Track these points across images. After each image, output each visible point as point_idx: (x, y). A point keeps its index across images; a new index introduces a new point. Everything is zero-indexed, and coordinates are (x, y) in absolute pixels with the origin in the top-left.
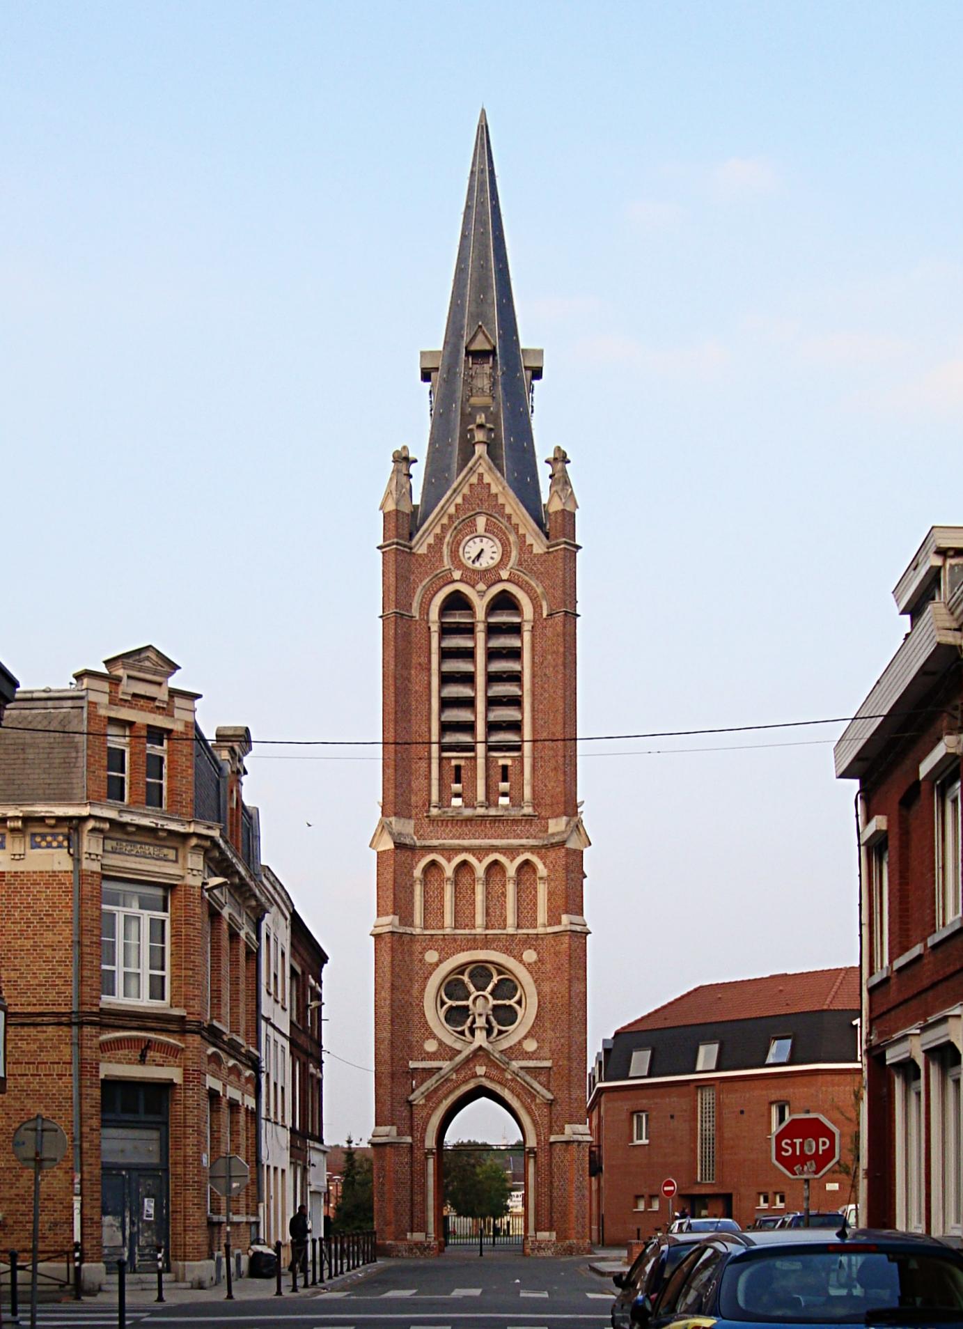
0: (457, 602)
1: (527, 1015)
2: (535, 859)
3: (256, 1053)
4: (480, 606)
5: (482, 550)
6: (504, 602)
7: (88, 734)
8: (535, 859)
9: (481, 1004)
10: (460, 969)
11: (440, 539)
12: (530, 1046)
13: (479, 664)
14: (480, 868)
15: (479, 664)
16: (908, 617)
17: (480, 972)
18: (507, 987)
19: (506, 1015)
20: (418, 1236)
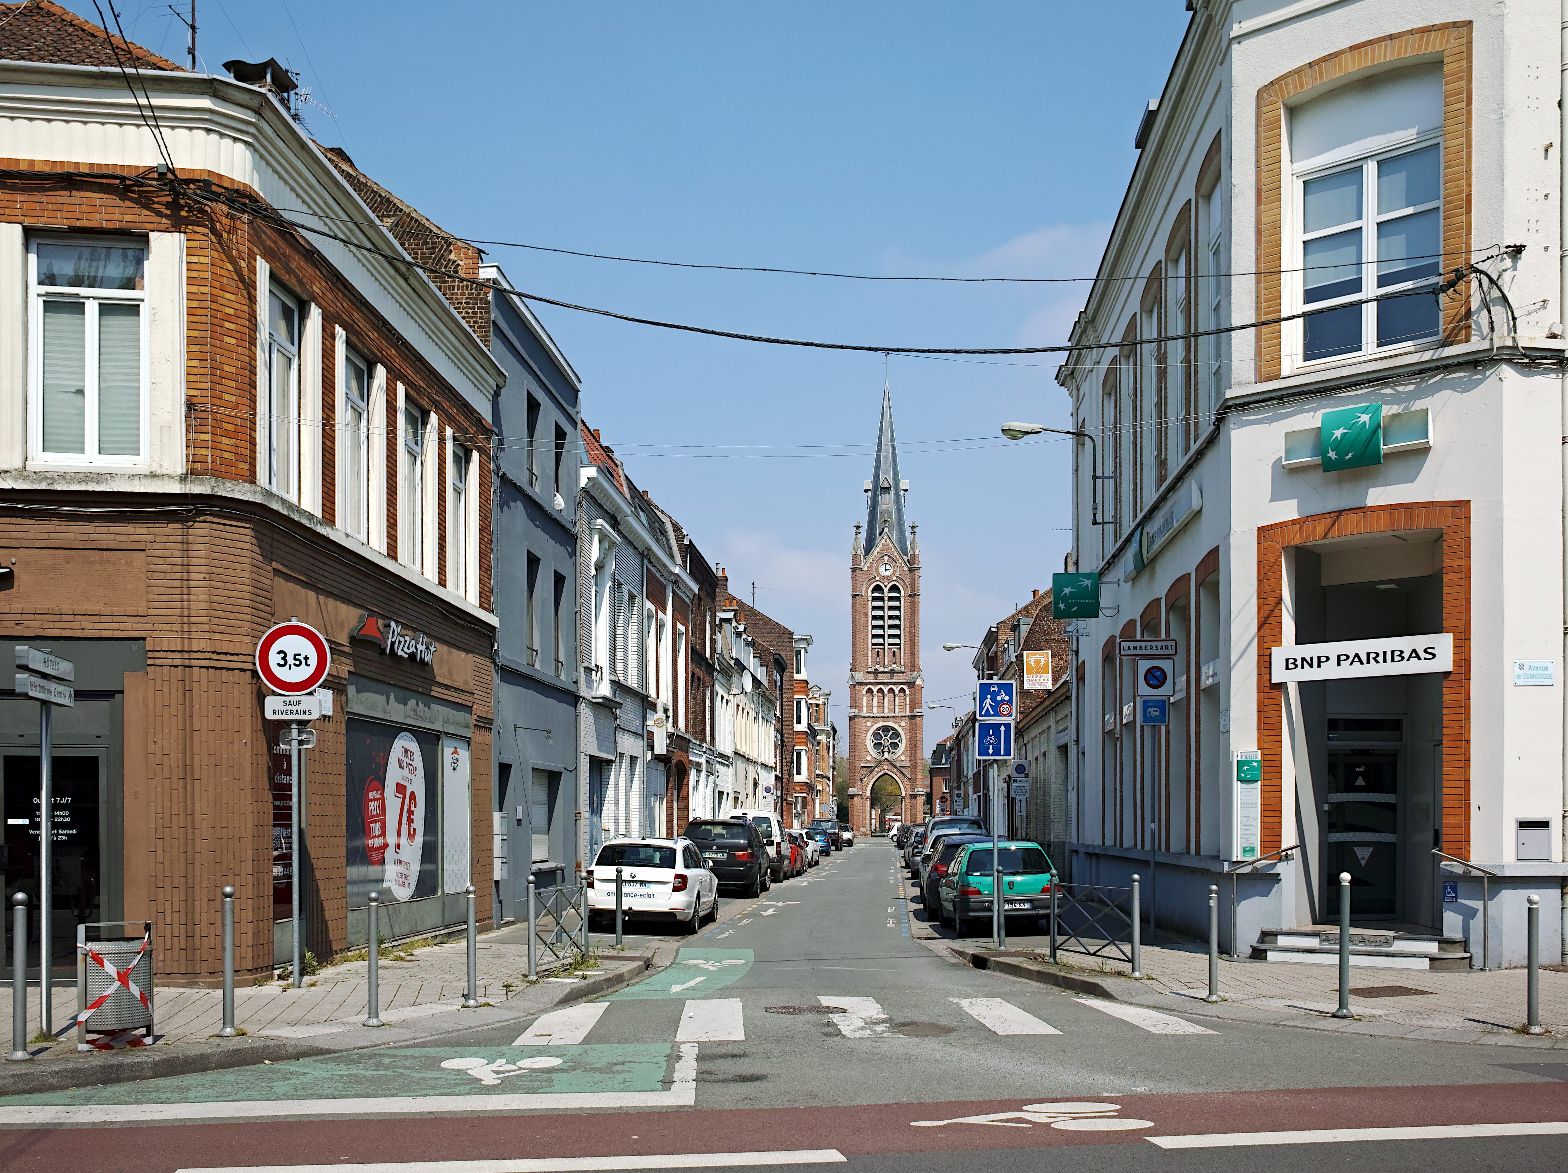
0: (878, 588)
1: (902, 746)
2: (905, 687)
3: (697, 671)
4: (886, 590)
5: (885, 570)
6: (894, 588)
7: (1279, 321)
8: (905, 687)
9: (886, 741)
10: (879, 729)
11: (872, 564)
12: (903, 758)
13: (888, 609)
14: (897, 690)
15: (888, 609)
16: (1130, 584)
17: (886, 729)
18: (896, 734)
19: (895, 746)
20: (864, 830)
